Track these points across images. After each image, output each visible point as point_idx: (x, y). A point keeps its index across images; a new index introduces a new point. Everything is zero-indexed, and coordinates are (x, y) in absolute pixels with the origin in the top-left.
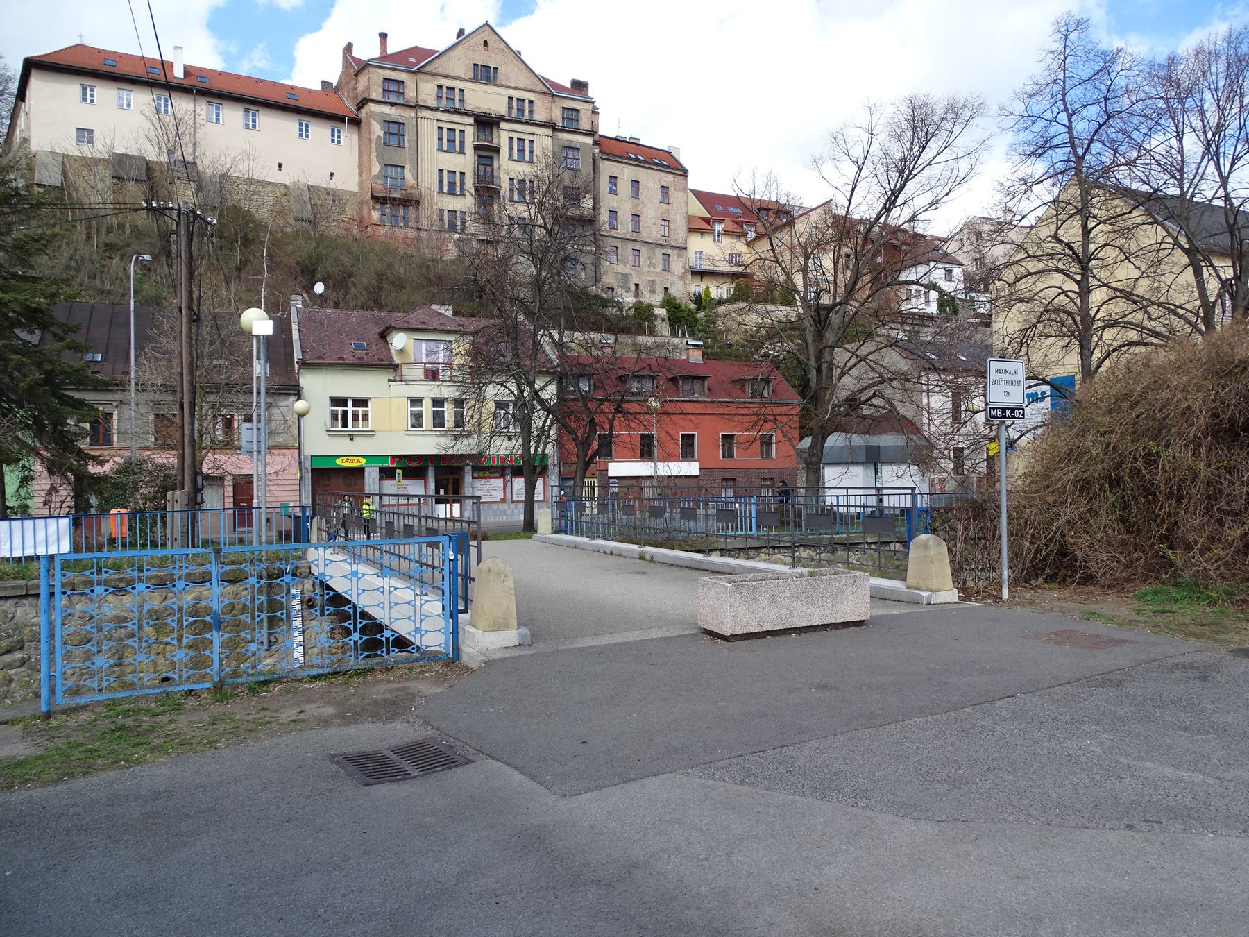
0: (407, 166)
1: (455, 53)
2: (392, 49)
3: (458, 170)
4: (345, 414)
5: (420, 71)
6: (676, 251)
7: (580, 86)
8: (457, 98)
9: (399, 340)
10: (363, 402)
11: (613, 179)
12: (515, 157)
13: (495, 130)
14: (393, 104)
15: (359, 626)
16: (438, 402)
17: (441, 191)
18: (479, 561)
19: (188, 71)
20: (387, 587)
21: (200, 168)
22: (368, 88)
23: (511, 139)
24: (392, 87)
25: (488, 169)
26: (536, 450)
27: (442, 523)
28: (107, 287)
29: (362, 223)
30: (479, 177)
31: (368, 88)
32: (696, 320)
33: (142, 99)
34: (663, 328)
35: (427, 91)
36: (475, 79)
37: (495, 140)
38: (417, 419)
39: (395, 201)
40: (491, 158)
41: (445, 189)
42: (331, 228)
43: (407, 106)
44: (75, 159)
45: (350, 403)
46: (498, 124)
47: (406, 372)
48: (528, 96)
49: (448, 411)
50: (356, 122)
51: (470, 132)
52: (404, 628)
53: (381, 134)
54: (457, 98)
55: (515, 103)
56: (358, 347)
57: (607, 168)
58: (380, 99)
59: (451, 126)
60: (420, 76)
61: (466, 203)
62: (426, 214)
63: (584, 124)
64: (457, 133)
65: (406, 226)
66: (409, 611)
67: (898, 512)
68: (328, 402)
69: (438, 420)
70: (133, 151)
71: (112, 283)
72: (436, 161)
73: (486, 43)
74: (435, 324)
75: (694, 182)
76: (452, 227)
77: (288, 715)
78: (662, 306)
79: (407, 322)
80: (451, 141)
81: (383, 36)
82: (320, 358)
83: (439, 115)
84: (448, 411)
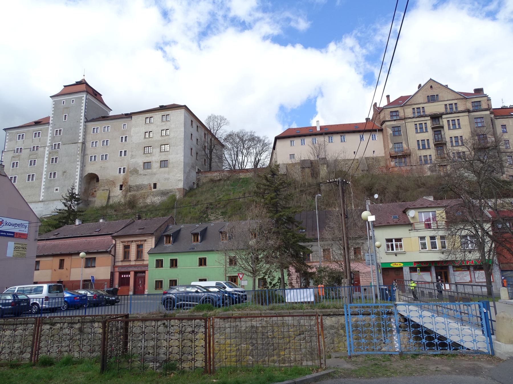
0: (404, 142)
1: (418, 94)
2: (392, 100)
3: (426, 139)
4: (392, 245)
5: (404, 105)
7: (479, 91)
8: (421, 111)
9: (412, 213)
10: (399, 240)
11: (504, 126)
12: (452, 128)
13: (440, 120)
14: (395, 120)
16: (433, 238)
17: (419, 149)
18: (496, 314)
19: (321, 128)
20: (446, 322)
21: (328, 159)
22: (384, 117)
23: (448, 121)
24: (394, 115)
25: (440, 136)
26: (489, 257)
27: (452, 293)
28: (302, 205)
29: (387, 167)
31: (384, 117)
33: (308, 140)
35: (409, 112)
36: (429, 102)
37: (441, 123)
38: (424, 246)
40: (440, 131)
41: (421, 148)
42: (376, 172)
43: (401, 119)
44: (290, 164)
45: (394, 241)
46: (441, 117)
47: (417, 226)
48: (453, 102)
49: (438, 242)
50: (381, 130)
51: (429, 123)
52: (456, 339)
53: (392, 132)
54: (421, 111)
55: (448, 106)
56: (395, 218)
57: (499, 122)
58: (390, 119)
59: (420, 123)
60: (404, 107)
61: (431, 152)
62: (414, 159)
63: (484, 106)
64: (423, 124)
65: (406, 166)
66: (457, 332)
68: (385, 241)
69: (434, 246)
70: (307, 158)
71: (303, 204)
72: (416, 137)
73: (431, 87)
74: (427, 204)
76: (426, 162)
77: (432, 368)
79: (414, 206)
80: (421, 128)
82: (380, 223)
83: (415, 120)
84: (438, 242)
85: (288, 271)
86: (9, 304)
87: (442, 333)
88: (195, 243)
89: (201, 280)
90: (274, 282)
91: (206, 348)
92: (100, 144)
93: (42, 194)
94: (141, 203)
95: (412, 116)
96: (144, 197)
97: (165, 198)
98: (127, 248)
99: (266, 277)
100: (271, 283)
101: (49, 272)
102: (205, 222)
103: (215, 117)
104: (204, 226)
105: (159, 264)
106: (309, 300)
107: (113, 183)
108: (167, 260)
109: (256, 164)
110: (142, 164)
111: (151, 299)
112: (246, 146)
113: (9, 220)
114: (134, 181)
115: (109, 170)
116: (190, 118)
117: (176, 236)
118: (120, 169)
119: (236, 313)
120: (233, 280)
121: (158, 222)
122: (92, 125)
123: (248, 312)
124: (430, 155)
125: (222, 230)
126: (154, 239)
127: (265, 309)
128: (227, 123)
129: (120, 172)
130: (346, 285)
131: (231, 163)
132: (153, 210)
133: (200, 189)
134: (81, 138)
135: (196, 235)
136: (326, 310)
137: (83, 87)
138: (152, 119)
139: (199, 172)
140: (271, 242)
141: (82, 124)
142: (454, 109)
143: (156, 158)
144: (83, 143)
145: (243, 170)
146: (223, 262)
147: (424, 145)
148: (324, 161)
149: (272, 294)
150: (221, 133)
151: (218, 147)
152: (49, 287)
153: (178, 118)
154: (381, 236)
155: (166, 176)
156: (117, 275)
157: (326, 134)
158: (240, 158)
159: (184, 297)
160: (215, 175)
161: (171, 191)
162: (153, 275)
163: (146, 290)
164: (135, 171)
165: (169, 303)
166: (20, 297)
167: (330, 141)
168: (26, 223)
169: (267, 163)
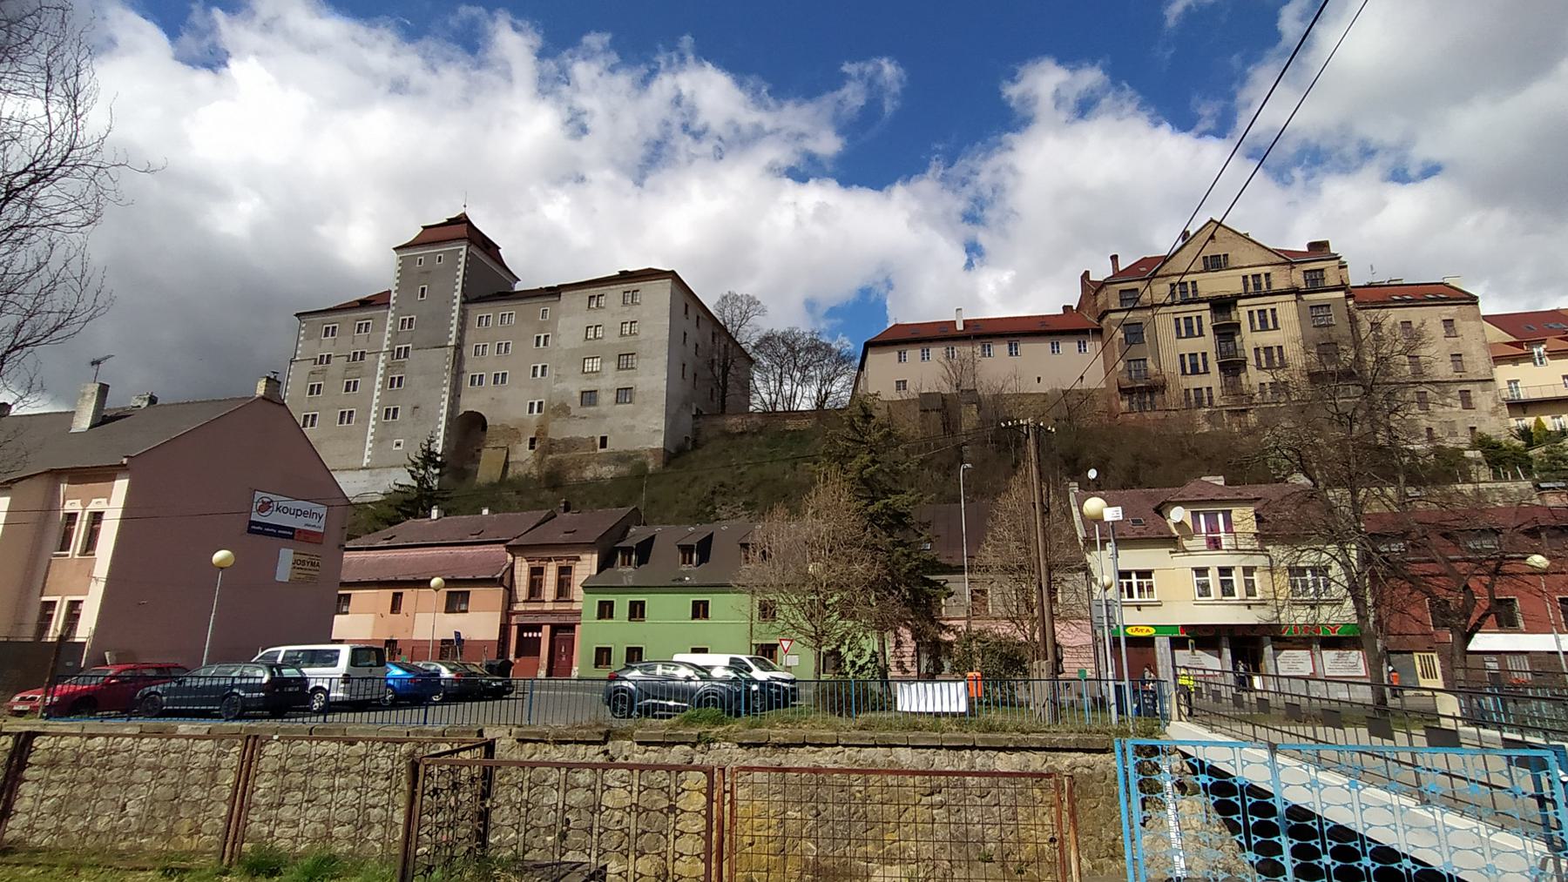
4: (1130, 585)
5: (1154, 275)
6: (1478, 385)
9: (1178, 514)
15: (1329, 848)
16: (1225, 571)
17: (1184, 372)
23: (1251, 313)
30: (1220, 352)
32: (1530, 459)
33: (937, 352)
34: (1485, 473)
35: (1161, 290)
36: (1207, 270)
37: (1234, 317)
38: (1204, 589)
39: (1144, 390)
42: (1086, 422)
48: (1263, 270)
49: (1237, 578)
50: (1098, 332)
51: (1207, 317)
55: (1250, 280)
57: (1365, 318)
61: (1213, 380)
62: (1173, 396)
63: (1332, 280)
67: (668, 536)
69: (1227, 589)
72: (1173, 346)
75: (1486, 308)
76: (1200, 404)
78: (1472, 448)
81: (1114, 258)
83: (1174, 309)
85: (897, 635)
86: (261, 687)
87: (1386, 838)
88: (685, 568)
89: (695, 651)
90: (860, 663)
91: (708, 838)
92: (491, 350)
93: (368, 452)
94: (572, 476)
96: (580, 467)
97: (624, 470)
98: (536, 572)
99: (843, 650)
100: (853, 664)
101: (369, 619)
102: (709, 522)
103: (736, 298)
104: (703, 530)
105: (606, 610)
106: (954, 709)
107: (514, 433)
108: (622, 603)
109: (821, 402)
110: (578, 395)
111: (585, 689)
112: (800, 363)
113: (284, 502)
114: (561, 430)
115: (507, 404)
116: (682, 298)
117: (644, 551)
118: (532, 404)
119: (779, 733)
120: (767, 653)
121: (604, 519)
122: (476, 311)
123: (805, 731)
124: (1209, 389)
125: (749, 540)
126: (596, 556)
127: (847, 725)
128: (763, 311)
129: (531, 411)
130: (1044, 677)
131: (766, 398)
132: (598, 493)
133: (700, 452)
134: (453, 336)
135: (686, 550)
136: (998, 735)
137: (462, 230)
138: (602, 301)
139: (698, 414)
140: (858, 567)
141: (457, 308)
142: (1264, 286)
143: (609, 381)
144: (459, 347)
145: (791, 414)
146: (746, 609)
148: (972, 396)
149: (866, 690)
150: (748, 337)
151: (740, 362)
152: (354, 652)
153: (658, 296)
154: (1104, 564)
155: (628, 421)
156: (514, 630)
157: (978, 337)
158: (786, 387)
159: (655, 688)
160: (733, 423)
161: (637, 454)
162: (590, 634)
163: (575, 668)
164: (563, 410)
165: (620, 701)
166: (288, 672)
167: (986, 351)
168: (323, 510)
169: (846, 397)
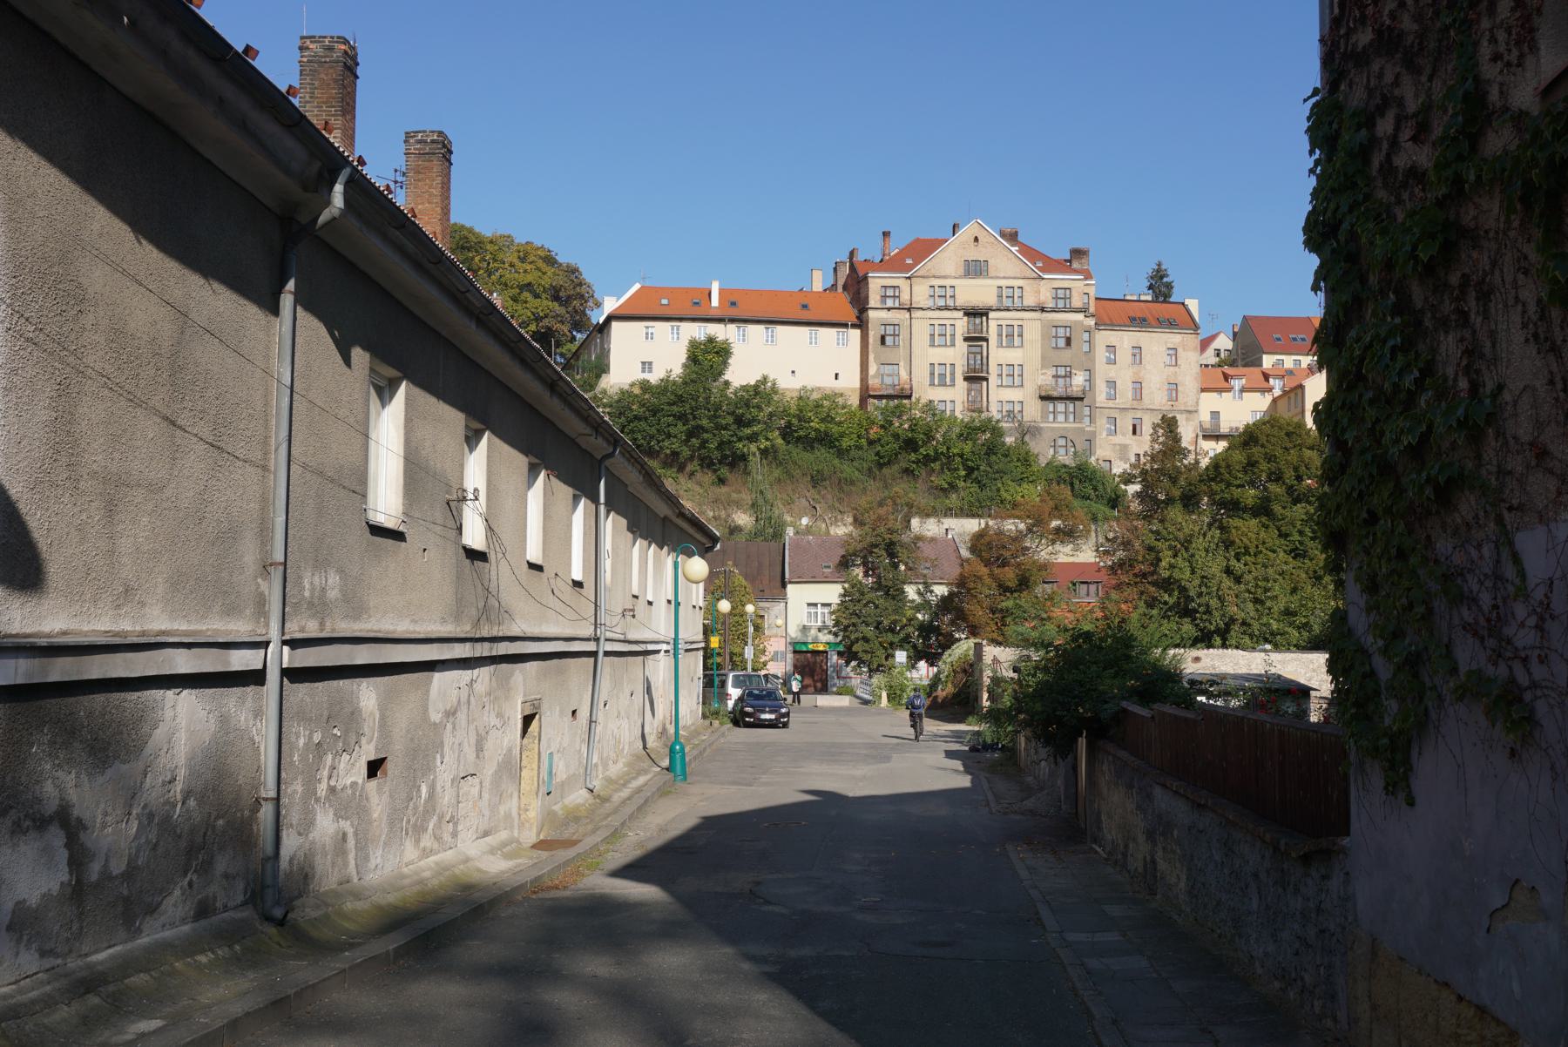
11: (1111, 348)
73: (976, 239)
95: (930, 303)
147: (943, 376)
